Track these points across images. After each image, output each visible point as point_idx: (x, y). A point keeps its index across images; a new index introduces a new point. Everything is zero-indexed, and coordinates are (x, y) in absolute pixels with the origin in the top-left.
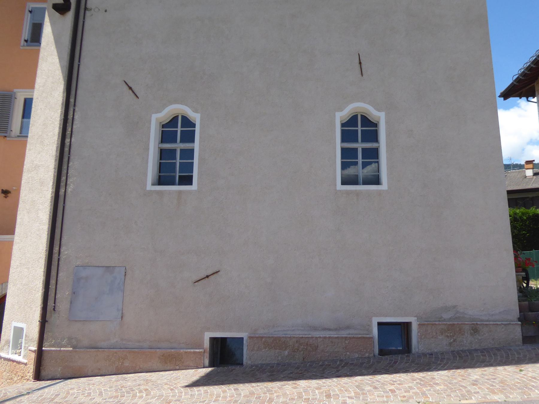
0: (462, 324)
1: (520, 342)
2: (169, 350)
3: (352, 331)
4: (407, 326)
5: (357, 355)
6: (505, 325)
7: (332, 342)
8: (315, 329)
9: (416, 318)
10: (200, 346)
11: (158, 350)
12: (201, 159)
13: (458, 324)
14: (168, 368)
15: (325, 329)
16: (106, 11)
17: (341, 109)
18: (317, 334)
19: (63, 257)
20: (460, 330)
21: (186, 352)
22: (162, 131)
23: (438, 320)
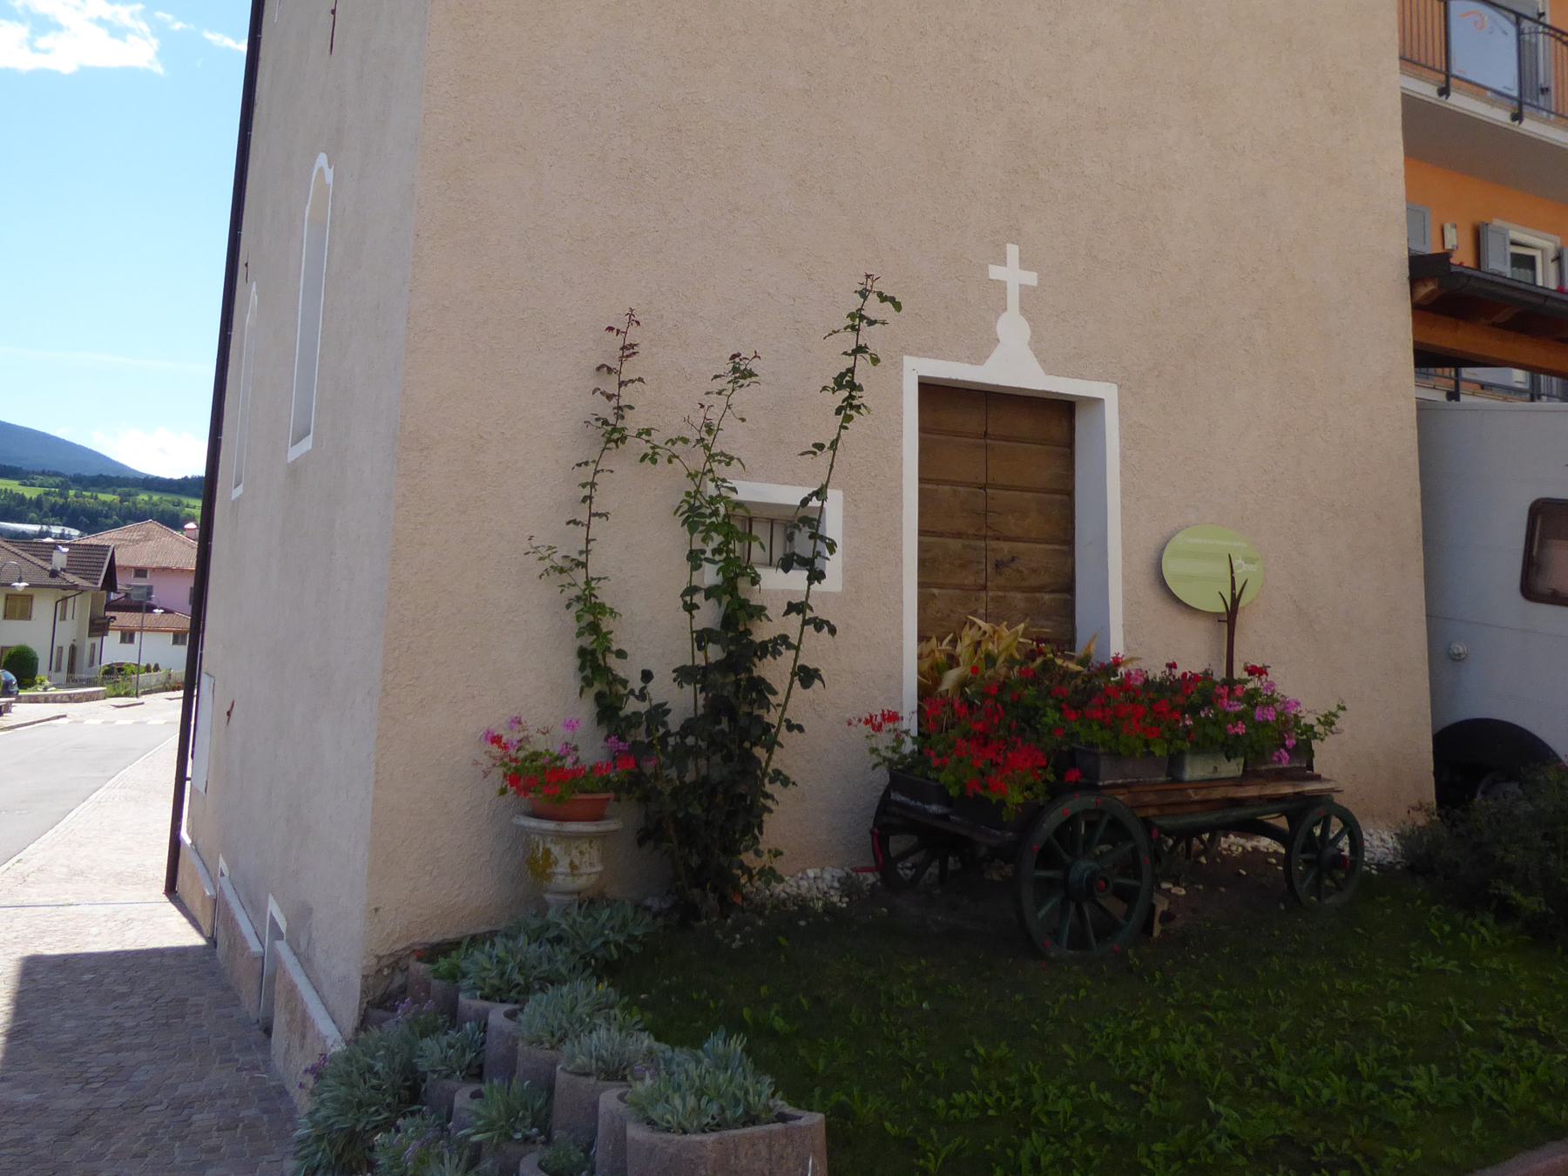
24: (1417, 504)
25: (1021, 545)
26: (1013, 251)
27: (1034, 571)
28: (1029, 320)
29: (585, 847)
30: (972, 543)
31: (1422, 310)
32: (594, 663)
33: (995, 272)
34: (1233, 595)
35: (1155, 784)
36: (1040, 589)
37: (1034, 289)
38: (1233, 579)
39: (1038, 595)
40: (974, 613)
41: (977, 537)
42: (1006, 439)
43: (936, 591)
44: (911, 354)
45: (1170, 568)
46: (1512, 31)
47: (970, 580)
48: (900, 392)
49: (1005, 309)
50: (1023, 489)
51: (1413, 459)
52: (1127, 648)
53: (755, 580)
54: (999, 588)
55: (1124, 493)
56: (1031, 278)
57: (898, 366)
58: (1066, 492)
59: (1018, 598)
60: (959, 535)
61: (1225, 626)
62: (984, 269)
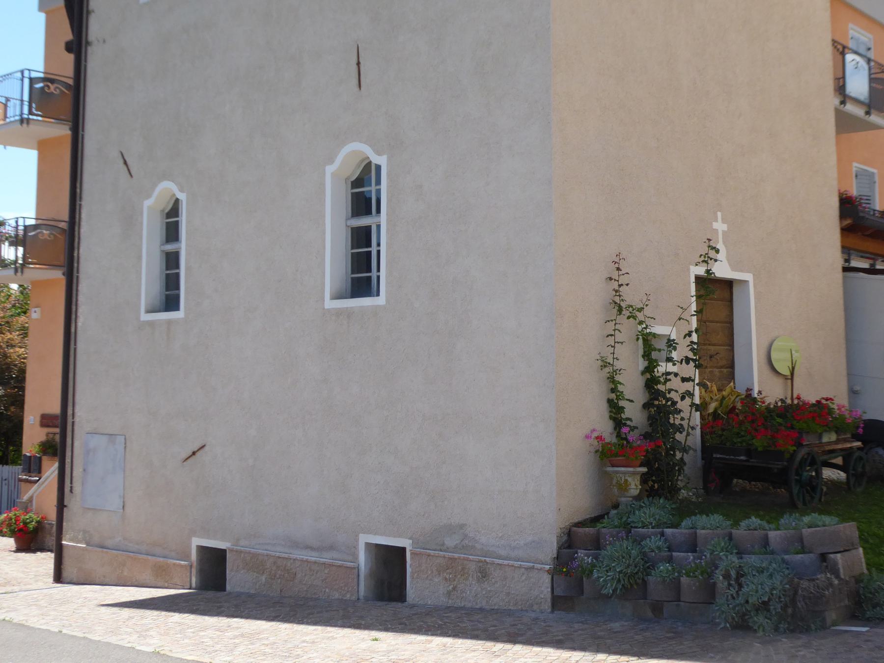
0: (464, 559)
1: (547, 606)
2: (161, 559)
3: (335, 554)
4: (404, 549)
5: (337, 596)
6: (527, 569)
7: (310, 570)
8: (295, 544)
9: (411, 541)
10: (186, 556)
11: (150, 557)
12: (188, 269)
13: (459, 558)
14: (159, 584)
15: (308, 547)
16: (104, 41)
17: (331, 161)
18: (299, 555)
19: (77, 419)
20: (463, 569)
21: (174, 564)
22: (167, 275)
23: (438, 548)
24: (843, 320)
32: (615, 409)
36: (721, 367)
46: (866, 67)
50: (717, 322)
51: (842, 302)
58: (729, 323)
59: (716, 371)
61: (789, 381)
62: (711, 224)
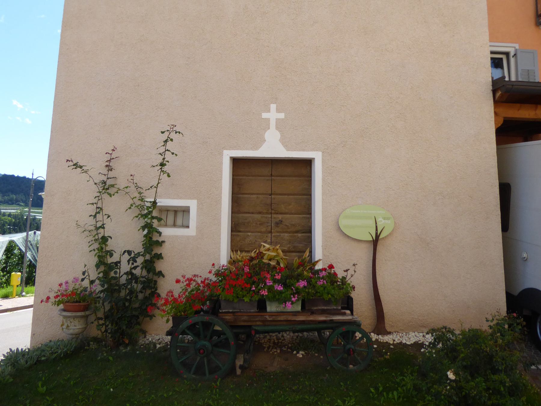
25: (288, 216)
26: (273, 107)
27: (294, 225)
28: (280, 131)
29: (72, 320)
30: (265, 216)
31: (497, 102)
33: (265, 115)
34: (377, 233)
35: (250, 312)
37: (283, 119)
38: (376, 227)
39: (296, 234)
40: (265, 242)
41: (267, 213)
42: (282, 176)
43: (249, 234)
44: (227, 149)
45: (343, 223)
47: (264, 229)
48: (221, 163)
49: (269, 128)
50: (288, 195)
52: (324, 255)
53: (160, 234)
54: (278, 232)
55: (324, 194)
56: (282, 116)
57: (221, 154)
60: (260, 213)
